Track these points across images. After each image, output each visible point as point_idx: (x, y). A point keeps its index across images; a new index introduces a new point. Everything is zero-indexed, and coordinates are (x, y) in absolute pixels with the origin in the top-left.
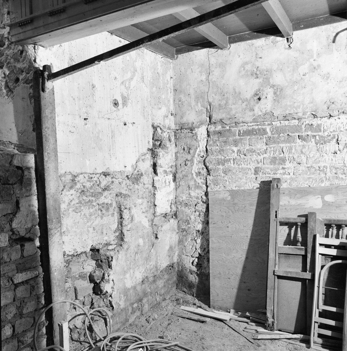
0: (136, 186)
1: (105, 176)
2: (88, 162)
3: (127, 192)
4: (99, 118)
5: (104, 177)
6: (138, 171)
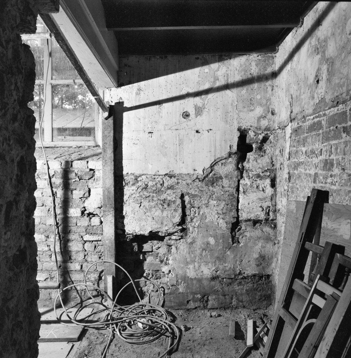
0: (211, 188)
1: (171, 177)
2: (150, 166)
3: (196, 193)
4: (165, 130)
5: (168, 178)
6: (215, 174)
